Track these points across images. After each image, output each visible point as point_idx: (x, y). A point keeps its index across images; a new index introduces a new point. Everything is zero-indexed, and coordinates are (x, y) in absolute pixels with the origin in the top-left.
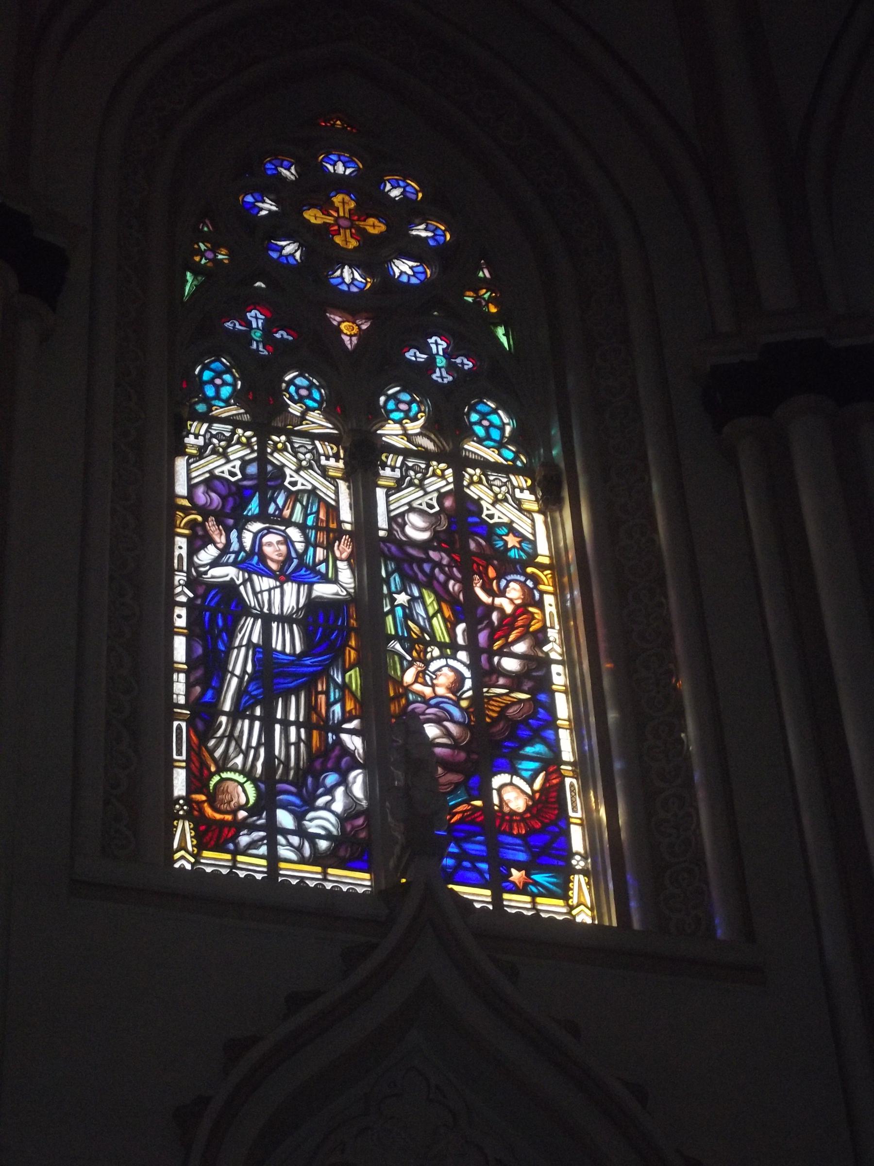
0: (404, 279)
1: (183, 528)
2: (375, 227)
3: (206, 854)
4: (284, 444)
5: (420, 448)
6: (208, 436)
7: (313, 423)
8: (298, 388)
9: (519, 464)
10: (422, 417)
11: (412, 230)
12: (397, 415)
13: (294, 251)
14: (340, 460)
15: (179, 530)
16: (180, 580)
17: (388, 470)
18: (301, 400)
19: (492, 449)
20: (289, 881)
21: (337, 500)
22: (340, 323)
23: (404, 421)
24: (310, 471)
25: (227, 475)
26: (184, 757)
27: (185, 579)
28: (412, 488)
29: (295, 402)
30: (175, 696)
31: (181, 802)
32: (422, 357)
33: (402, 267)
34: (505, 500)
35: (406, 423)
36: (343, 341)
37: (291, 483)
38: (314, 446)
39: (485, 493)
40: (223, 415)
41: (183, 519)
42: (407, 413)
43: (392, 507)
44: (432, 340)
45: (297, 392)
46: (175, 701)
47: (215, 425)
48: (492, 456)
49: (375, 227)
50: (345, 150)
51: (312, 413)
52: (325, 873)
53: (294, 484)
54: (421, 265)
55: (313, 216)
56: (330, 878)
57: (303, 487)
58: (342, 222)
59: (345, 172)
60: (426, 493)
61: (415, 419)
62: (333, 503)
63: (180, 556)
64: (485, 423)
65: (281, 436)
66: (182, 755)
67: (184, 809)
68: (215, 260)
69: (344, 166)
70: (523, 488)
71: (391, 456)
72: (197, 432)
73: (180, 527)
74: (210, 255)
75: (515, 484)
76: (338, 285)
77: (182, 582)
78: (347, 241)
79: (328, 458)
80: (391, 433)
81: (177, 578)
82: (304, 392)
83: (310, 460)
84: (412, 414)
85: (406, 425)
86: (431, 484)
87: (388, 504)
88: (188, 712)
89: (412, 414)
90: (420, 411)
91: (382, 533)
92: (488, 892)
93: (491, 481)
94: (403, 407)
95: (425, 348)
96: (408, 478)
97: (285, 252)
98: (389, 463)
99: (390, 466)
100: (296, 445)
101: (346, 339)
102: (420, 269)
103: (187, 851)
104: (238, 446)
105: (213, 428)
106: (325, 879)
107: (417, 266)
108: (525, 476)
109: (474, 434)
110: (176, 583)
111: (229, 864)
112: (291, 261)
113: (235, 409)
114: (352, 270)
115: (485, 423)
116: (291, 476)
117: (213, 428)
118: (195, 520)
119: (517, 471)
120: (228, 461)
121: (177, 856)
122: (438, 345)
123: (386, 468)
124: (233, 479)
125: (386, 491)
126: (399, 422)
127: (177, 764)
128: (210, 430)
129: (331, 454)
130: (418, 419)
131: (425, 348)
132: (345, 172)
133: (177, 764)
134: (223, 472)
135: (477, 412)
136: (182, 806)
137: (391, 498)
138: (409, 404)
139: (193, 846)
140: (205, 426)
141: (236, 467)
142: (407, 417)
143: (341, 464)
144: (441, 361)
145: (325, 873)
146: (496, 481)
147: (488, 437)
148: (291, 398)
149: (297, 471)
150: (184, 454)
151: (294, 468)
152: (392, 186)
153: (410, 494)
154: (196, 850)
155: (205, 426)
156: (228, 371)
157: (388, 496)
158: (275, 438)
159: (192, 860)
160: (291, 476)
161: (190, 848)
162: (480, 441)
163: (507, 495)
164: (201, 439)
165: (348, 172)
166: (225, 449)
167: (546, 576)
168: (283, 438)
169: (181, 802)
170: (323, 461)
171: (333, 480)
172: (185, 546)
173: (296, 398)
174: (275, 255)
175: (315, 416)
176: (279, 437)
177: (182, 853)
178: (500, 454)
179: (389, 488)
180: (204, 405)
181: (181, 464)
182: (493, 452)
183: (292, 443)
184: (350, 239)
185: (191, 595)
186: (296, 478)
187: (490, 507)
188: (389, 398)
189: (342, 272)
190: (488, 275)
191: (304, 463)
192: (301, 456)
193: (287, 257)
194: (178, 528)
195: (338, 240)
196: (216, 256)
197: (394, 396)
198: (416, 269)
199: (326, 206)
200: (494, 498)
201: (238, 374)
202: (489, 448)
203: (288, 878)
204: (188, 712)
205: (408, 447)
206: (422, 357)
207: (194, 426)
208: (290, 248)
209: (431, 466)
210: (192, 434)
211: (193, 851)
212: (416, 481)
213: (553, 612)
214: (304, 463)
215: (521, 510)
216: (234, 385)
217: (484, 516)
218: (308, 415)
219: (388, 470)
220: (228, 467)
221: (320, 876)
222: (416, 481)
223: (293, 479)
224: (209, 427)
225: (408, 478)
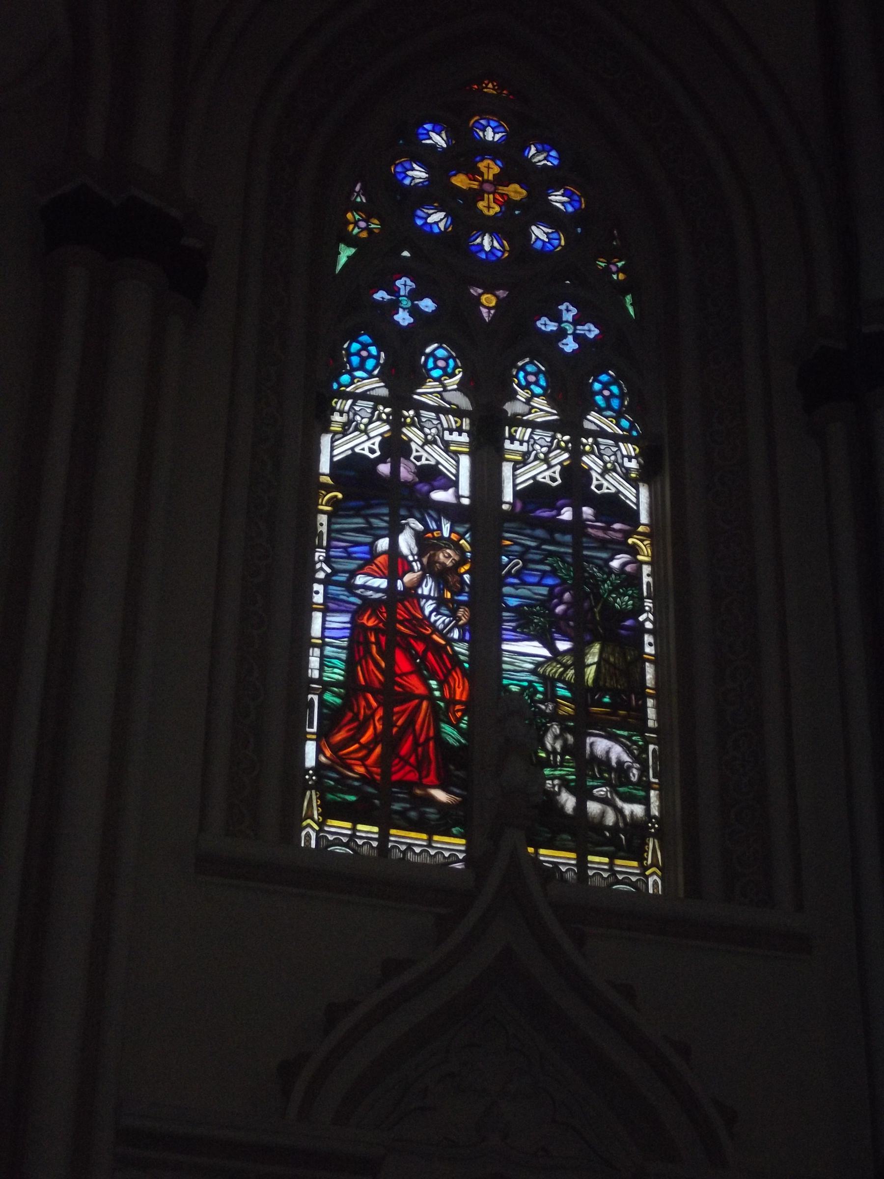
0: (539, 245)
1: (326, 505)
2: (516, 192)
3: (331, 822)
4: (412, 419)
5: (453, 406)
6: (532, 441)
7: (541, 410)
8: (527, 374)
9: (635, 433)
10: (459, 372)
11: (426, 178)
12: (436, 373)
13: (439, 219)
14: (335, 413)
15: (320, 507)
16: (320, 556)
17: (517, 443)
18: (527, 387)
19: (610, 419)
20: (457, 855)
21: (638, 503)
22: (480, 295)
23: (443, 379)
24: (435, 446)
25: (366, 452)
26: (315, 730)
27: (324, 554)
28: (357, 433)
29: (523, 388)
30: (310, 671)
31: (311, 772)
32: (552, 327)
33: (539, 232)
34: (434, 442)
35: (445, 380)
36: (481, 312)
37: (416, 458)
38: (439, 422)
39: (595, 463)
40: (539, 420)
41: (325, 496)
42: (444, 369)
43: (518, 481)
44: (562, 307)
45: (525, 378)
46: (310, 675)
47: (359, 401)
48: (610, 427)
49: (516, 192)
50: (494, 114)
51: (536, 399)
52: (430, 840)
53: (418, 458)
54: (557, 232)
55: (460, 181)
56: (434, 845)
57: (427, 462)
58: (487, 187)
59: (493, 138)
60: (370, 438)
61: (453, 375)
62: (453, 478)
63: (321, 532)
64: (606, 393)
65: (409, 411)
66: (313, 728)
67: (313, 780)
68: (370, 231)
69: (493, 131)
70: (631, 455)
71: (340, 401)
72: (521, 438)
73: (322, 505)
74: (363, 224)
75: (625, 453)
76: (477, 252)
77: (321, 558)
78: (489, 207)
79: (451, 431)
80: (427, 393)
81: (317, 554)
82: (532, 378)
83: (434, 435)
84: (449, 370)
85: (446, 382)
86: (556, 457)
87: (515, 477)
88: (321, 687)
89: (449, 370)
90: (456, 367)
91: (505, 507)
92: (573, 855)
93: (423, 422)
94: (441, 363)
95: (557, 317)
96: (534, 452)
97: (430, 220)
98: (338, 407)
99: (339, 411)
100: (424, 420)
101: (484, 311)
102: (555, 236)
103: (313, 819)
104: (378, 423)
105: (357, 404)
106: (430, 846)
107: (552, 232)
108: (634, 445)
109: (595, 404)
110: (316, 559)
111: (349, 832)
112: (436, 230)
113: (374, 382)
114: (492, 238)
115: (606, 393)
116: (417, 451)
117: (357, 404)
118: (336, 497)
119: (626, 439)
120: (550, 467)
121: (304, 823)
122: (569, 312)
123: (515, 442)
124: (372, 456)
125: (513, 465)
126: (438, 380)
127: (309, 736)
128: (354, 407)
129: (633, 454)
130: (456, 375)
131: (557, 317)
132: (493, 138)
133: (309, 736)
134: (363, 449)
135: (600, 382)
136: (311, 776)
137: (518, 472)
138: (446, 360)
139: (319, 815)
140: (350, 402)
141: (557, 473)
142: (445, 373)
143: (465, 438)
144: (405, 302)
145: (430, 840)
146: (540, 440)
147: (609, 407)
148: (519, 385)
149: (602, 475)
150: (327, 431)
151: (420, 443)
152: (537, 150)
153: (535, 468)
154: (321, 818)
155: (350, 402)
156: (614, 381)
157: (515, 469)
158: (405, 413)
159: (317, 828)
160: (417, 451)
161: (316, 817)
162: (600, 411)
163: (437, 437)
164: (525, 444)
165: (497, 137)
166: (546, 454)
167: (645, 546)
168: (591, 440)
169: (311, 772)
170: (447, 436)
171: (634, 483)
172: (325, 523)
173: (523, 383)
174: (419, 222)
175: (540, 403)
176: (587, 439)
177: (309, 821)
178: (618, 425)
179: (516, 462)
180: (348, 383)
181: (507, 469)
182: (612, 422)
183: (598, 444)
184: (493, 205)
185: (329, 571)
186: (422, 453)
187: (419, 449)
188: (428, 356)
189: (483, 239)
190: (364, 201)
191: (429, 437)
192: (427, 431)
193: (431, 224)
194: (320, 505)
195: (481, 205)
196: (368, 225)
197: (432, 354)
198: (551, 236)
199: (473, 172)
200: (603, 467)
201: (461, 363)
202: (607, 417)
203: (340, 836)
204: (321, 687)
205: (617, 432)
206: (552, 327)
207: (339, 404)
208: (436, 217)
209: (556, 438)
210: (337, 411)
211: (319, 819)
212: (542, 456)
213: (323, 532)
214: (429, 437)
215: (447, 451)
216: (377, 358)
217: (593, 487)
218: (533, 400)
219: (517, 443)
220: (367, 445)
221: (425, 843)
222: (542, 456)
223: (418, 454)
224: (353, 404)
225: (534, 452)
